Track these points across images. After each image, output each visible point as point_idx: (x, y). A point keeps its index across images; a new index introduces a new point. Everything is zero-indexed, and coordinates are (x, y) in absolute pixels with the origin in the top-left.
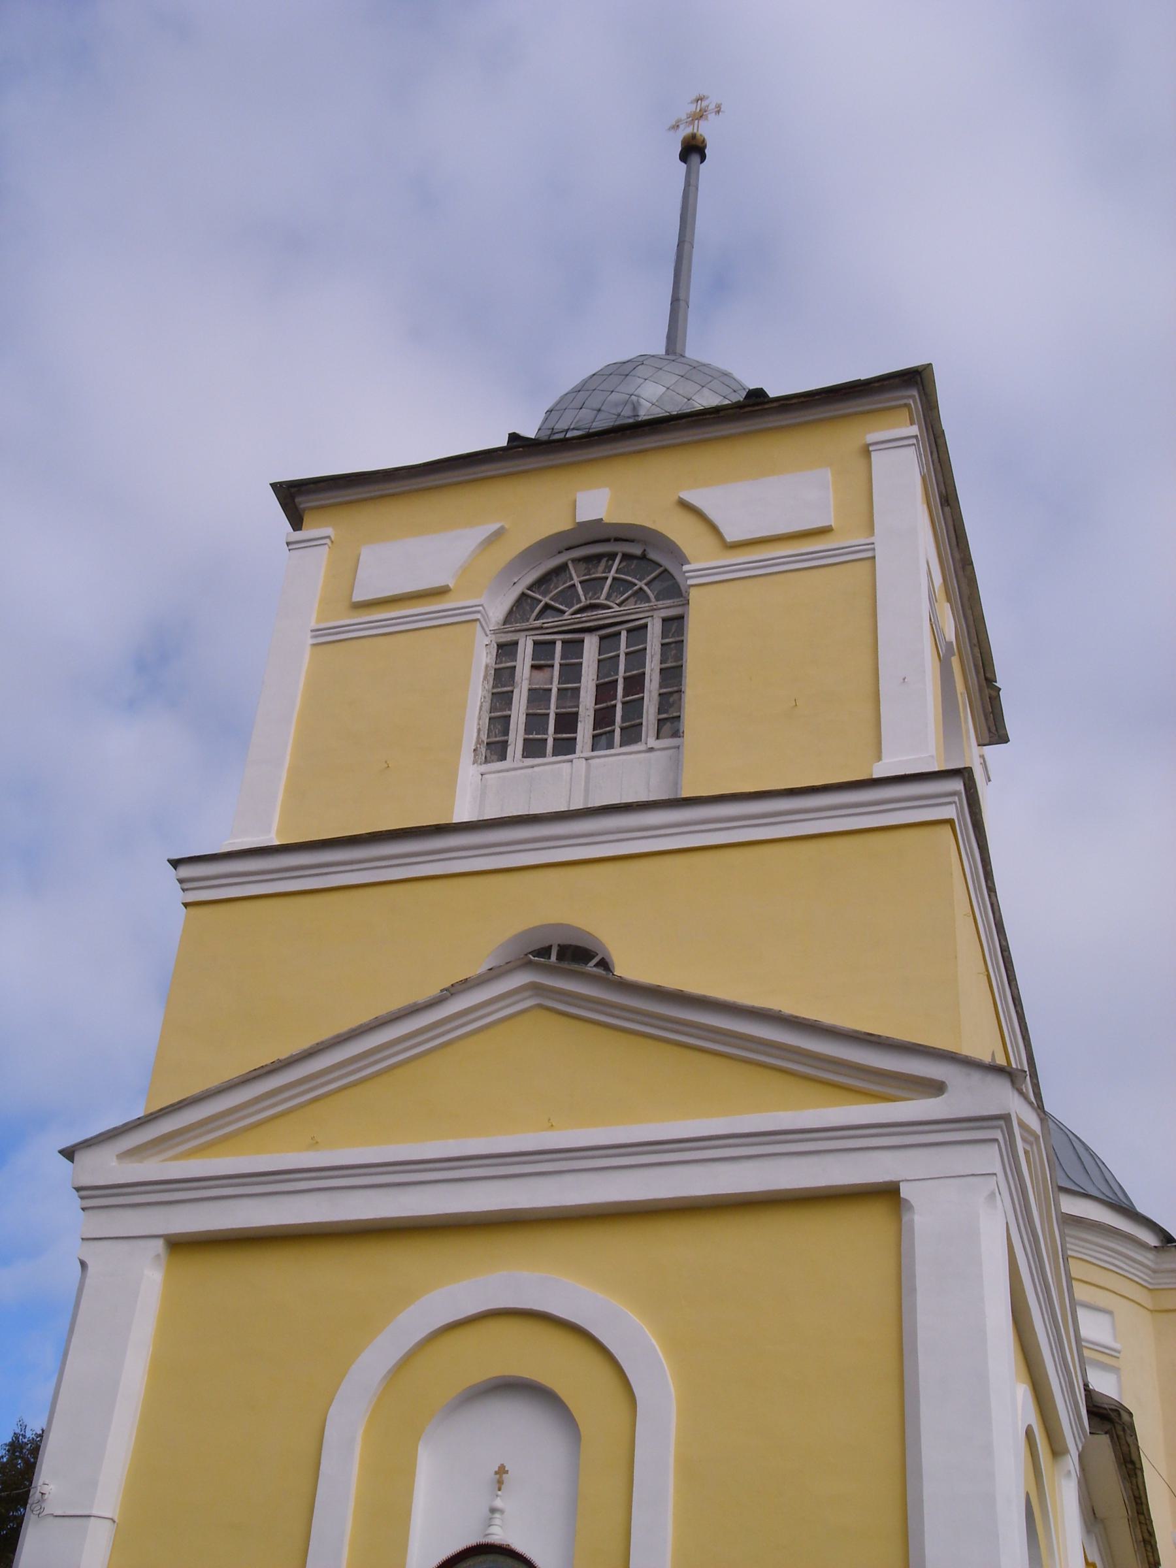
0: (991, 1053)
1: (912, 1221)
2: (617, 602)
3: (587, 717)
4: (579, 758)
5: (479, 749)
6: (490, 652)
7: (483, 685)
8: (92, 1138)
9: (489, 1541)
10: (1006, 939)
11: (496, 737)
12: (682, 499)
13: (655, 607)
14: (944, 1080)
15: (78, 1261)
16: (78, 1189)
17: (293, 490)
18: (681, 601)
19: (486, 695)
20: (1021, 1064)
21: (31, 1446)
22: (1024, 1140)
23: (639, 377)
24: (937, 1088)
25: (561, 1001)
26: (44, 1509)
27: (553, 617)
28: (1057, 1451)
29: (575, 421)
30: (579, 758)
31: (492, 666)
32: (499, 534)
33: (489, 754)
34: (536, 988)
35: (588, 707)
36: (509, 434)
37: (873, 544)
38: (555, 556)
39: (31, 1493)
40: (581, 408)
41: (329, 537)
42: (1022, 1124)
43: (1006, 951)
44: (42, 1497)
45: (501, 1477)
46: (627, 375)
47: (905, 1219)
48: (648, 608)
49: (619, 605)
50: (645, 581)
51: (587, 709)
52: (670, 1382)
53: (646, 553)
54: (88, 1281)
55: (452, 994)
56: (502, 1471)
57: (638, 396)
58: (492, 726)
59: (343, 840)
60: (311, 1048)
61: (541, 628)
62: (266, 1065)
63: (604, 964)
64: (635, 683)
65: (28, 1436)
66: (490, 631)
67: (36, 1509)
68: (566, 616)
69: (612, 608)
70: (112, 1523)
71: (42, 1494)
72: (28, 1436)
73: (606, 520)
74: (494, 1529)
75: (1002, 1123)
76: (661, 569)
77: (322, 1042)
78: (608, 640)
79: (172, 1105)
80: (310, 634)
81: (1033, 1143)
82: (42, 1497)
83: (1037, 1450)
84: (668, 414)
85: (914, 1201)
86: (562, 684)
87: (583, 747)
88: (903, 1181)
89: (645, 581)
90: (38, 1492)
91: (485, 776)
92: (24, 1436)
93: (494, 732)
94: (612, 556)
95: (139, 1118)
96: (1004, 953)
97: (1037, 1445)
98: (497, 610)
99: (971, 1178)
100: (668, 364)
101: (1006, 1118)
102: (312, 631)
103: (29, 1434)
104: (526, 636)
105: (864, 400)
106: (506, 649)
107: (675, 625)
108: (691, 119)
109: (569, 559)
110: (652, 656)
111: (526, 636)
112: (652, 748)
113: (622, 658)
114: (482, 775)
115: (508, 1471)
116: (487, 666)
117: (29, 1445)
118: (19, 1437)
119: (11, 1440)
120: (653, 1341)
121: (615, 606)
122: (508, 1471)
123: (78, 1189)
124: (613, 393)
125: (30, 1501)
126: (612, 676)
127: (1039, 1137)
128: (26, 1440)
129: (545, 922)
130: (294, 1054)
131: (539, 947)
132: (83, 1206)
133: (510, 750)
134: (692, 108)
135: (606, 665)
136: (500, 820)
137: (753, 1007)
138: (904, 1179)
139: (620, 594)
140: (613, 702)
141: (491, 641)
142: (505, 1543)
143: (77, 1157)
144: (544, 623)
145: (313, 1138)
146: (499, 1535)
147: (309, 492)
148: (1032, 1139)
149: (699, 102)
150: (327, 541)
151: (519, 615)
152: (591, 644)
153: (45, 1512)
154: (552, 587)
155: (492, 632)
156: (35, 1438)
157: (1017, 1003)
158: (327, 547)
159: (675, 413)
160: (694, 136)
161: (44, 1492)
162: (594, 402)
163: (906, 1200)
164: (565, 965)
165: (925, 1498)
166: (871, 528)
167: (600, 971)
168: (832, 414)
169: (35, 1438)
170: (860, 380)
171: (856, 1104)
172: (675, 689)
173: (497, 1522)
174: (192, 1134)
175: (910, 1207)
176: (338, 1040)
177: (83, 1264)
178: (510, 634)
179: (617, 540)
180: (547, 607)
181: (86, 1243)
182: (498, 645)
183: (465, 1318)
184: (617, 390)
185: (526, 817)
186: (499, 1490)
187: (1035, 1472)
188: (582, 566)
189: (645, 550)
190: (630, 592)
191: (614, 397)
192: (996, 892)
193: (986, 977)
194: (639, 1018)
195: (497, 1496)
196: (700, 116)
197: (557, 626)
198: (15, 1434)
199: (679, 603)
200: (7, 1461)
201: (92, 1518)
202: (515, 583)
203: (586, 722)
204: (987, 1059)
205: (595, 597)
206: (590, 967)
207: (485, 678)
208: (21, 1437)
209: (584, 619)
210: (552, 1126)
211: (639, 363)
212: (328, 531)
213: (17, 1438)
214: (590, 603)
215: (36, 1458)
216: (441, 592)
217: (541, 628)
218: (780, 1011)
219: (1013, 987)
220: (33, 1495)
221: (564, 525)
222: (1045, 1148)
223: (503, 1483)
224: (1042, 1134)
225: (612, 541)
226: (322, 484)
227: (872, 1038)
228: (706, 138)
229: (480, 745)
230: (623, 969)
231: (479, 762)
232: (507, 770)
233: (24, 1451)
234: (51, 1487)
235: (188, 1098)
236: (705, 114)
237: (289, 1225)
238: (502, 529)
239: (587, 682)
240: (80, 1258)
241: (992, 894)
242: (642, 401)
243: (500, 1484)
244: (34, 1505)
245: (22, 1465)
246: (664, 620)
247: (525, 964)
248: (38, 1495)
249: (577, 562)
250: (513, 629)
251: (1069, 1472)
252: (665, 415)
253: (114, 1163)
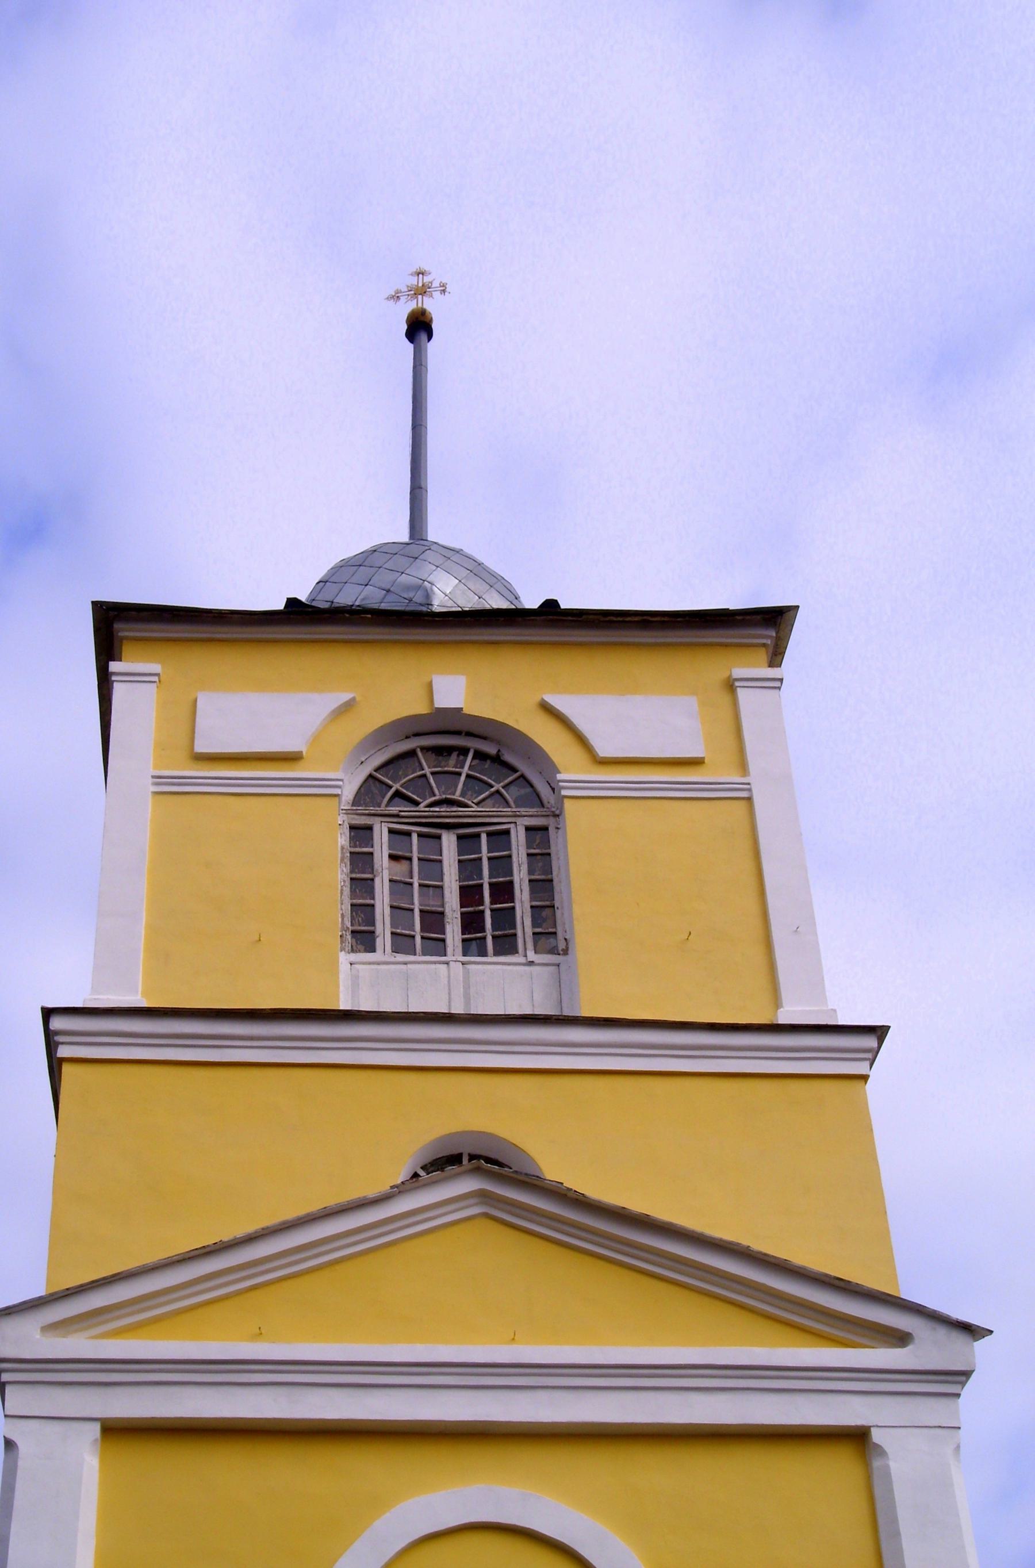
1: (887, 1468)
2: (475, 801)
3: (455, 920)
4: (455, 961)
5: (345, 936)
6: (344, 833)
7: (340, 867)
8: (14, 1306)
11: (360, 925)
12: (545, 701)
13: (518, 813)
14: (911, 1332)
17: (112, 614)
18: (546, 811)
19: (346, 879)
23: (430, 563)
24: (901, 1339)
27: (405, 807)
29: (360, 597)
30: (455, 961)
31: (347, 849)
32: (348, 707)
33: (355, 944)
34: (483, 1196)
35: (455, 909)
36: (288, 599)
37: (749, 784)
38: (403, 740)
40: (366, 585)
41: (157, 675)
46: (417, 558)
48: (510, 813)
49: (477, 804)
50: (502, 784)
51: (454, 911)
53: (500, 754)
57: (432, 584)
58: (354, 913)
59: (240, 1013)
61: (397, 816)
62: (208, 1246)
64: (504, 891)
66: (342, 810)
68: (421, 807)
69: (472, 807)
73: (466, 711)
76: (517, 774)
77: (268, 1228)
78: (467, 841)
79: (104, 1278)
80: (151, 780)
84: (460, 609)
86: (463, 881)
87: (454, 950)
88: (874, 1426)
89: (502, 784)
91: (353, 965)
93: (357, 920)
94: (464, 751)
95: (67, 1289)
98: (349, 791)
99: (937, 1429)
100: (455, 554)
102: (153, 777)
104: (381, 822)
105: (717, 632)
106: (360, 833)
107: (537, 833)
108: (412, 292)
109: (418, 747)
110: (520, 866)
111: (381, 822)
112: (533, 962)
113: (485, 863)
114: (351, 964)
116: (342, 848)
121: (473, 805)
124: (403, 574)
126: (474, 880)
129: (467, 1129)
130: (238, 1236)
131: (448, 1154)
133: (379, 942)
134: (413, 281)
135: (468, 867)
136: (414, 1015)
137: (721, 1240)
138: (875, 1424)
139: (475, 793)
140: (481, 908)
141: (344, 821)
144: (400, 811)
147: (127, 620)
149: (421, 276)
150: (156, 679)
151: (369, 798)
152: (449, 841)
154: (400, 773)
155: (344, 811)
158: (155, 684)
159: (467, 609)
160: (423, 312)
162: (384, 579)
166: (743, 767)
168: (679, 640)
170: (728, 609)
171: (811, 1347)
172: (548, 903)
176: (283, 1226)
178: (363, 817)
179: (469, 734)
180: (398, 794)
181: (9, 1420)
182: (350, 827)
184: (406, 572)
185: (441, 1015)
188: (432, 756)
189: (499, 751)
190: (487, 793)
191: (404, 579)
196: (422, 291)
197: (420, 817)
199: (544, 813)
202: (362, 762)
203: (454, 924)
205: (449, 792)
207: (342, 860)
209: (444, 814)
211: (427, 548)
212: (155, 668)
214: (446, 798)
216: (291, 758)
217: (397, 816)
218: (749, 1246)
221: (421, 708)
225: (463, 734)
226: (145, 614)
227: (842, 1284)
228: (434, 318)
229: (346, 931)
231: (347, 950)
232: (378, 964)
235: (122, 1272)
236: (428, 290)
238: (353, 699)
239: (451, 882)
240: (6, 1436)
242: (435, 589)
246: (528, 829)
249: (425, 751)
250: (367, 812)
252: (454, 609)
253: (38, 1335)
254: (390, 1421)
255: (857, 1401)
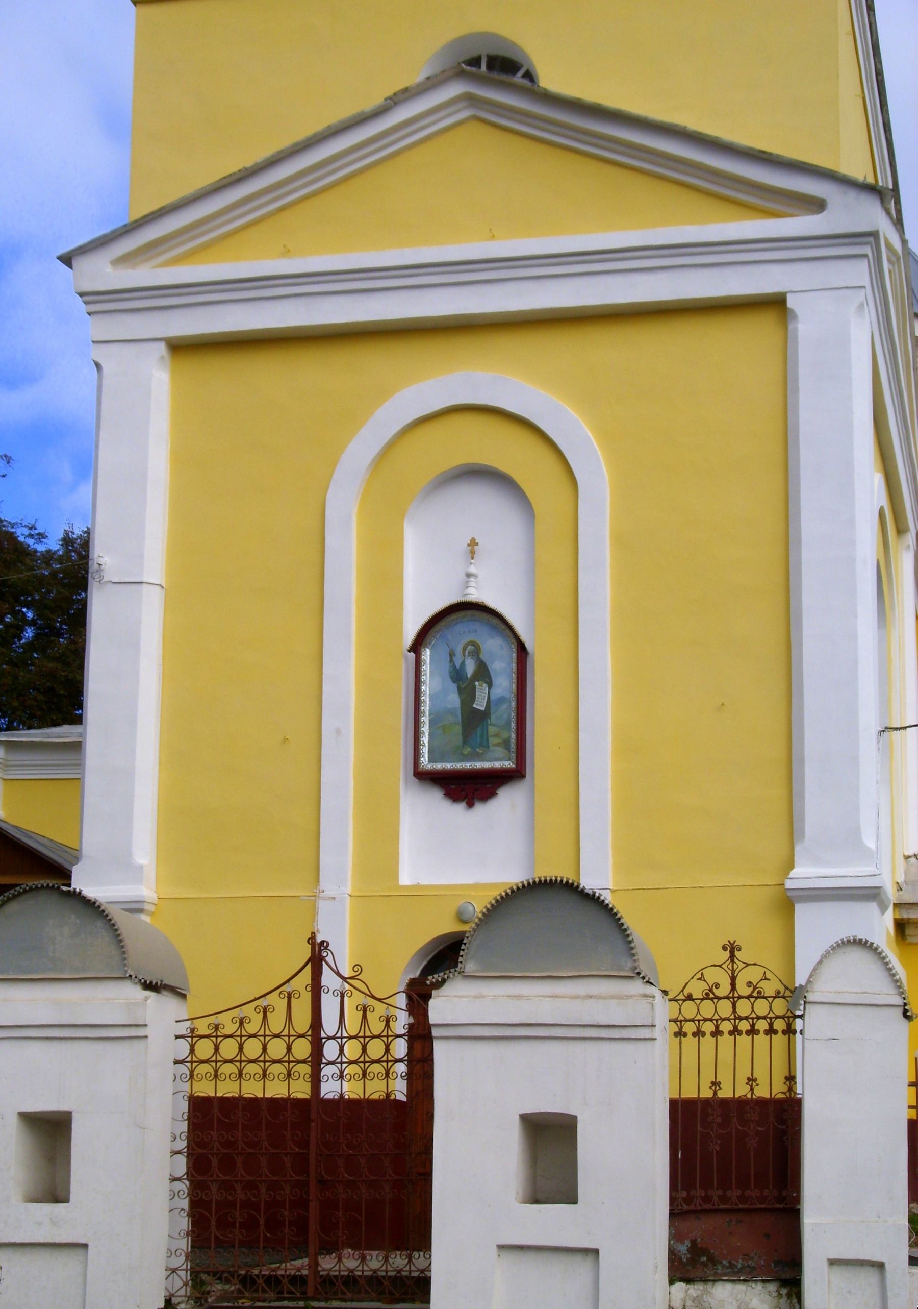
0: (864, 176)
1: (796, 329)
9: (468, 600)
10: (881, 63)
15: (93, 362)
16: (81, 295)
20: (887, 183)
21: (80, 541)
22: (889, 260)
24: (817, 205)
25: (494, 113)
26: (103, 577)
28: (901, 530)
34: (469, 99)
39: (90, 565)
42: (889, 246)
43: (880, 75)
44: (100, 568)
45: (473, 548)
47: (790, 327)
52: (604, 468)
54: (105, 381)
55: (395, 104)
56: (473, 543)
60: (273, 156)
62: (234, 173)
63: (529, 76)
65: (76, 533)
67: (96, 577)
70: (162, 588)
71: (99, 565)
72: (76, 533)
74: (470, 590)
75: (871, 239)
79: (153, 213)
81: (895, 264)
82: (100, 568)
83: (887, 528)
85: (798, 312)
88: (789, 292)
90: (95, 563)
92: (73, 533)
96: (879, 77)
97: (888, 531)
101: (875, 235)
103: (78, 532)
115: (478, 543)
117: (79, 540)
118: (69, 534)
119: (62, 536)
120: (590, 434)
122: (478, 543)
123: (81, 295)
125: (90, 570)
127: (900, 257)
128: (75, 536)
132: (88, 311)
137: (662, 122)
142: (480, 601)
143: (75, 263)
145: (284, 246)
146: (475, 595)
148: (894, 259)
153: (103, 581)
156: (82, 534)
157: (887, 129)
161: (100, 563)
163: (792, 311)
164: (495, 75)
165: (803, 560)
167: (526, 83)
169: (82, 534)
173: (472, 584)
174: (178, 240)
175: (795, 317)
177: (98, 366)
183: (433, 413)
186: (472, 559)
187: (884, 544)
192: (874, 11)
193: (862, 100)
194: (562, 131)
195: (471, 564)
198: (65, 530)
200: (63, 554)
201: (144, 585)
204: (860, 178)
206: (518, 79)
208: (70, 534)
210: (493, 236)
213: (67, 534)
215: (88, 551)
219: (885, 114)
220: (91, 566)
222: (905, 268)
223: (475, 553)
224: (903, 254)
227: (765, 156)
230: (548, 81)
233: (75, 545)
234: (106, 559)
237: (272, 329)
241: (871, 13)
243: (472, 554)
244: (95, 574)
245: (75, 557)
247: (460, 74)
248: (96, 566)
251: (909, 546)
253: (109, 269)
254: (413, 318)
255: (129, 319)
